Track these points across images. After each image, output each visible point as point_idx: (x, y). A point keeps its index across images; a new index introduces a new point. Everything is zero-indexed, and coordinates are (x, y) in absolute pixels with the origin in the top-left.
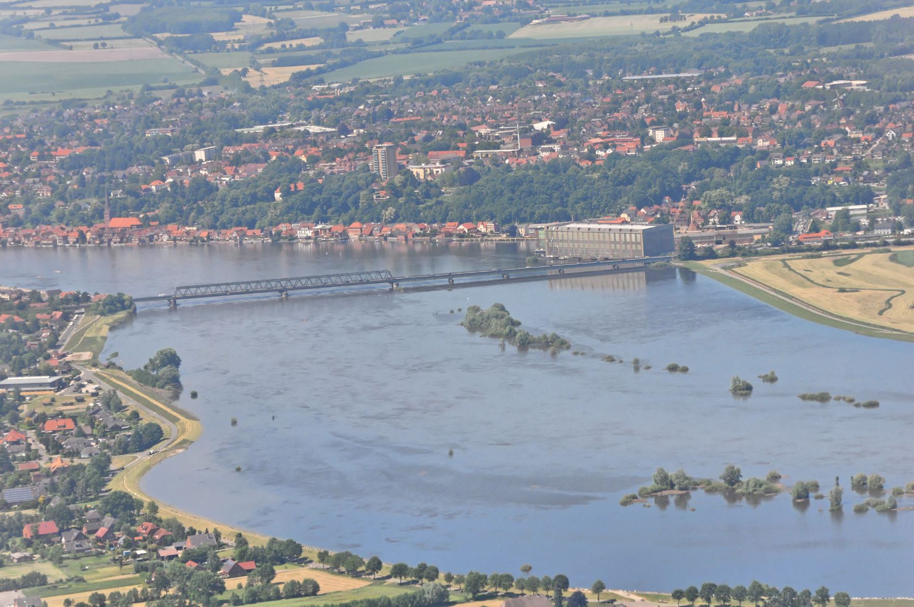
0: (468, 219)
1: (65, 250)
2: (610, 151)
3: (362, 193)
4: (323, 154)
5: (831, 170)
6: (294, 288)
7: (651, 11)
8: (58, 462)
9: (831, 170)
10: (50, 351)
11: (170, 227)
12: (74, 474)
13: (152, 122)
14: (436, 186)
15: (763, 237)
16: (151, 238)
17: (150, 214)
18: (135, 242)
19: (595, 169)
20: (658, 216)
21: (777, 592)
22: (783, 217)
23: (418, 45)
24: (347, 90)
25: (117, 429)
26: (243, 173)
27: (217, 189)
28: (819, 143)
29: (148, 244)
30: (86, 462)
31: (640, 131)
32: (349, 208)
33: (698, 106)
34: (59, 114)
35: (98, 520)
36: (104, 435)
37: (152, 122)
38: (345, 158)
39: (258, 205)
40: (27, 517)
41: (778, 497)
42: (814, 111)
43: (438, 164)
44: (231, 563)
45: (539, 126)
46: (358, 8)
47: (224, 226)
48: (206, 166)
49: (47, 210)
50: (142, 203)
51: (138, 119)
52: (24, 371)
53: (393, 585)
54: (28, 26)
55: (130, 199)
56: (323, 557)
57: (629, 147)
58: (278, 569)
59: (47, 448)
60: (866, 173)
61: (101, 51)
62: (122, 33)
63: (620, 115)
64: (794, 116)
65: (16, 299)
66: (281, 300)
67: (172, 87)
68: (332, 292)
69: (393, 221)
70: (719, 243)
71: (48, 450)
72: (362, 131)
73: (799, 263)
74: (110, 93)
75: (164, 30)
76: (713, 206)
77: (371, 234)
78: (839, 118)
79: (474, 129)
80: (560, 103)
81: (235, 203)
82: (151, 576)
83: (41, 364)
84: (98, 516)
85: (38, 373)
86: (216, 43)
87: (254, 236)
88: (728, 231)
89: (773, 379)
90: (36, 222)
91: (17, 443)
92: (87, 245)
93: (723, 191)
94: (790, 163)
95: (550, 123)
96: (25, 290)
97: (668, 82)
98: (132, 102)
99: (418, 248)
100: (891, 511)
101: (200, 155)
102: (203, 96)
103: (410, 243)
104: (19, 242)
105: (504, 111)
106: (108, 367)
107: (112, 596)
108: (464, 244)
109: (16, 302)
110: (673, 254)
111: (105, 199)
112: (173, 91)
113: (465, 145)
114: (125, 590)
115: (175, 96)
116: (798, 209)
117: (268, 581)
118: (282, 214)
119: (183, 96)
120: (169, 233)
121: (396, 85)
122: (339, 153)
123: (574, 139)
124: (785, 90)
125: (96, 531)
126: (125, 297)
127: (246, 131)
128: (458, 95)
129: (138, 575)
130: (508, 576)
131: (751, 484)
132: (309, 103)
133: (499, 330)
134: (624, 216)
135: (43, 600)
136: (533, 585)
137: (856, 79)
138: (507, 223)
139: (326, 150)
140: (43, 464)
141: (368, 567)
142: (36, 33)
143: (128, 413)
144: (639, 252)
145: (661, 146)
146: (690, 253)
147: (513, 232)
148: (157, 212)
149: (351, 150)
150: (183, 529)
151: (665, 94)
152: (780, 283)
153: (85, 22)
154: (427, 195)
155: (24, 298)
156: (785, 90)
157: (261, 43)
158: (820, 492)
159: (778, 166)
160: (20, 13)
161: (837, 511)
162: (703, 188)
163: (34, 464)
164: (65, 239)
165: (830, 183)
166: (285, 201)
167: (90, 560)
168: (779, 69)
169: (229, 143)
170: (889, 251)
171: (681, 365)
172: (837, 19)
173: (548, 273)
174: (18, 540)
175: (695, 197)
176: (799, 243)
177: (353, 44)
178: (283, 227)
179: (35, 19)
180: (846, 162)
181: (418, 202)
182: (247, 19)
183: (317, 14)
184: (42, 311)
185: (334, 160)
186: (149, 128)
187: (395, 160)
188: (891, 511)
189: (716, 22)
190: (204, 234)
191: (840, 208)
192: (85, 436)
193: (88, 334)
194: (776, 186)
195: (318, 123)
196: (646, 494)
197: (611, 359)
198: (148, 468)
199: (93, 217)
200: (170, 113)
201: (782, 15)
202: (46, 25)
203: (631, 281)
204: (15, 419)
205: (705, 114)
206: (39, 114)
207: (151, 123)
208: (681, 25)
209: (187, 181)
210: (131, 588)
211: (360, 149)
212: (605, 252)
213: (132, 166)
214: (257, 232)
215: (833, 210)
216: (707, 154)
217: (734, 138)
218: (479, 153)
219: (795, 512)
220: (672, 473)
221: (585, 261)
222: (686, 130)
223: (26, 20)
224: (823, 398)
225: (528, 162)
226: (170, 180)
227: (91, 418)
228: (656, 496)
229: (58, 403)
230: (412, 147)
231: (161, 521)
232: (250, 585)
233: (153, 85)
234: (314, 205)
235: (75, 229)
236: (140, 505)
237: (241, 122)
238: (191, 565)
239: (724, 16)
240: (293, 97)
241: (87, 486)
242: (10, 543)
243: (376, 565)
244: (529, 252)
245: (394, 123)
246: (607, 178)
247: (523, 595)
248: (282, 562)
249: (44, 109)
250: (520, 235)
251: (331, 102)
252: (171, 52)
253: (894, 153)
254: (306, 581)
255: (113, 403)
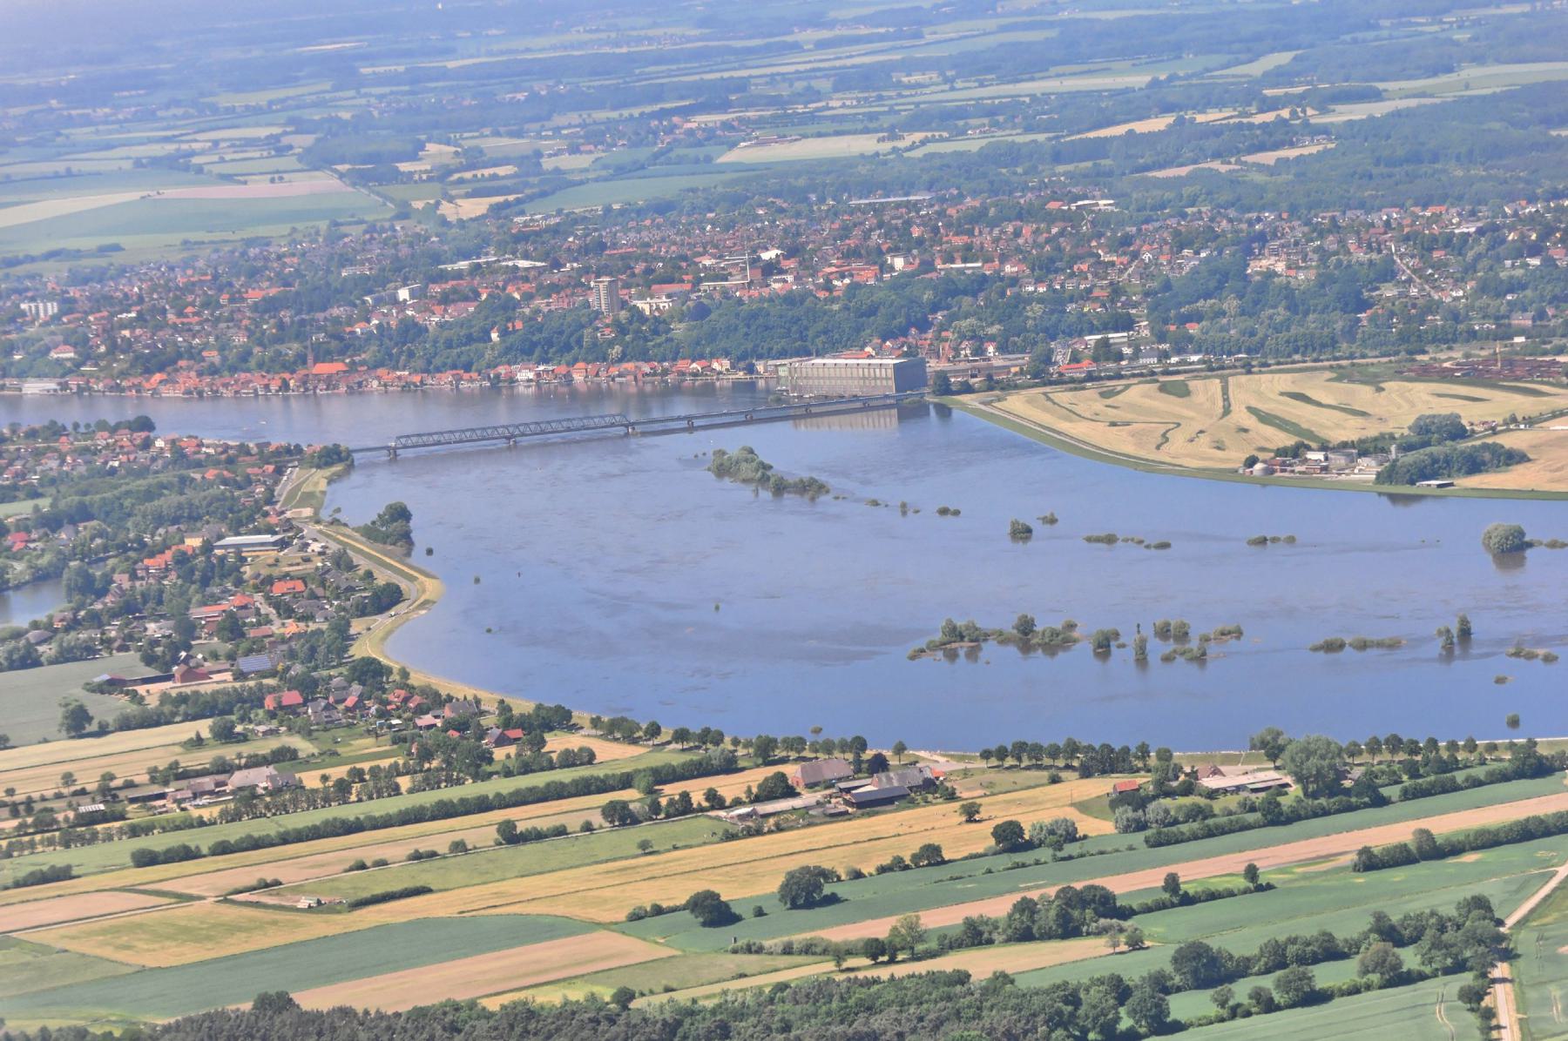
0: (701, 357)
1: (267, 398)
2: (847, 281)
3: (588, 331)
4: (537, 290)
5: (1087, 295)
6: (523, 435)
7: (866, 131)
8: (292, 627)
9: (1087, 295)
10: (266, 508)
11: (381, 371)
12: (313, 640)
13: (347, 260)
14: (664, 321)
15: (1022, 369)
16: (360, 384)
17: (357, 359)
18: (343, 389)
19: (834, 300)
20: (905, 349)
21: (1094, 749)
22: (1040, 348)
23: (621, 171)
24: (553, 221)
25: (351, 589)
26: (452, 313)
27: (427, 330)
28: (1071, 268)
29: (357, 390)
30: (325, 626)
31: (877, 258)
32: (572, 348)
33: (936, 230)
34: (243, 254)
35: (344, 688)
36: (337, 598)
37: (347, 260)
38: (562, 294)
39: (474, 346)
40: (268, 686)
41: (1078, 646)
42: (1062, 233)
43: (664, 299)
44: (497, 732)
45: (768, 255)
46: (550, 133)
47: (438, 370)
48: (412, 306)
49: (245, 356)
50: (347, 347)
51: (331, 258)
52: (242, 530)
53: (674, 751)
54: (196, 160)
55: (334, 344)
56: (596, 723)
57: (868, 276)
58: (548, 737)
59: (278, 613)
60: (1123, 298)
61: (278, 185)
62: (299, 166)
63: (852, 242)
64: (1041, 239)
65: (222, 453)
66: (509, 448)
67: (362, 222)
68: (563, 438)
69: (621, 360)
70: (973, 376)
71: (279, 615)
72: (575, 265)
73: (1063, 396)
74: (294, 230)
75: (343, 162)
76: (963, 337)
77: (597, 375)
78: (1089, 241)
79: (697, 260)
80: (785, 230)
81: (449, 345)
82: (410, 748)
83: (260, 521)
84: (345, 684)
85: (258, 531)
86: (403, 174)
87: (471, 380)
88: (982, 363)
89: (1053, 521)
90: (233, 369)
91: (245, 607)
92: (290, 393)
93: (972, 321)
94: (1042, 289)
95: (779, 252)
96: (231, 443)
97: (898, 205)
98: (321, 240)
99: (648, 388)
100: (1200, 659)
101: (403, 294)
102: (395, 231)
103: (640, 384)
104: (217, 391)
105: (725, 240)
106: (332, 523)
107: (372, 769)
108: (697, 383)
109: (223, 457)
110: (927, 390)
111: (308, 343)
112: (364, 226)
113: (690, 277)
114: (385, 763)
115: (366, 232)
116: (1053, 339)
117: (539, 750)
118: (500, 356)
119: (375, 231)
120: (378, 378)
121: (605, 215)
122: (555, 288)
123: (807, 268)
124: (1029, 213)
125: (344, 700)
126: (342, 448)
127: (449, 267)
128: (673, 224)
129: (395, 747)
130: (801, 739)
131: (1048, 634)
132: (514, 236)
133: (751, 475)
134: (868, 349)
135: (297, 776)
136: (828, 748)
137: (1103, 198)
138: (744, 359)
139: (540, 287)
140: (276, 628)
141: (646, 733)
142: (206, 168)
143: (361, 572)
144: (891, 387)
145: (903, 274)
146: (944, 387)
147: (751, 369)
148: (363, 356)
149: (568, 285)
150: (440, 695)
151: (899, 218)
152: (1047, 419)
153: (257, 154)
154: (656, 332)
155: (231, 452)
156: (1029, 213)
157: (450, 172)
158: (1121, 641)
159: (1029, 293)
160: (185, 147)
161: (1142, 660)
162: (952, 318)
163: (265, 629)
164: (267, 387)
165: (1086, 310)
166: (503, 341)
167: (340, 734)
168: (1016, 189)
169: (434, 281)
170: (1157, 381)
171: (952, 509)
172: (1068, 135)
173: (792, 412)
174: (261, 712)
175: (943, 327)
176: (1061, 375)
177: (550, 173)
178: (502, 370)
179: (202, 153)
180: (1102, 288)
181: (646, 340)
182: (432, 148)
183: (505, 141)
184: (253, 466)
185: (549, 296)
186: (344, 267)
187: (618, 295)
188: (1200, 659)
189: (937, 141)
190: (416, 379)
191: (1099, 337)
192: (317, 598)
193: (305, 488)
194: (1030, 314)
195: (526, 257)
196: (934, 647)
197: (875, 503)
198: (390, 633)
199: (295, 363)
200: (364, 250)
201: (1008, 132)
202: (215, 158)
203: (882, 420)
204: (239, 582)
205: (945, 239)
206: (221, 254)
207: (345, 261)
208: (901, 144)
209: (393, 323)
210: (392, 760)
211: (577, 284)
212: (855, 388)
213: (332, 307)
214: (474, 375)
215: (1092, 339)
216: (953, 282)
217: (979, 264)
218: (705, 285)
219: (1096, 664)
220: (960, 623)
221: (832, 398)
222: (926, 257)
223: (193, 153)
224: (1110, 540)
225: (760, 294)
226: (375, 322)
227: (321, 577)
228: (945, 650)
229: (283, 562)
230: (634, 280)
231: (413, 688)
232: (519, 755)
233: (339, 220)
234: (534, 345)
235: (277, 377)
236: (389, 671)
237: (443, 258)
238: (453, 734)
239: (945, 134)
240: (495, 230)
241: (329, 652)
242: (252, 716)
243: (654, 730)
244: (768, 391)
245: (610, 255)
246: (849, 309)
247: (817, 758)
248: (551, 729)
249: (226, 249)
250: (758, 373)
251: (538, 234)
252: (354, 185)
253: (1152, 277)
254: (581, 749)
255: (342, 562)
